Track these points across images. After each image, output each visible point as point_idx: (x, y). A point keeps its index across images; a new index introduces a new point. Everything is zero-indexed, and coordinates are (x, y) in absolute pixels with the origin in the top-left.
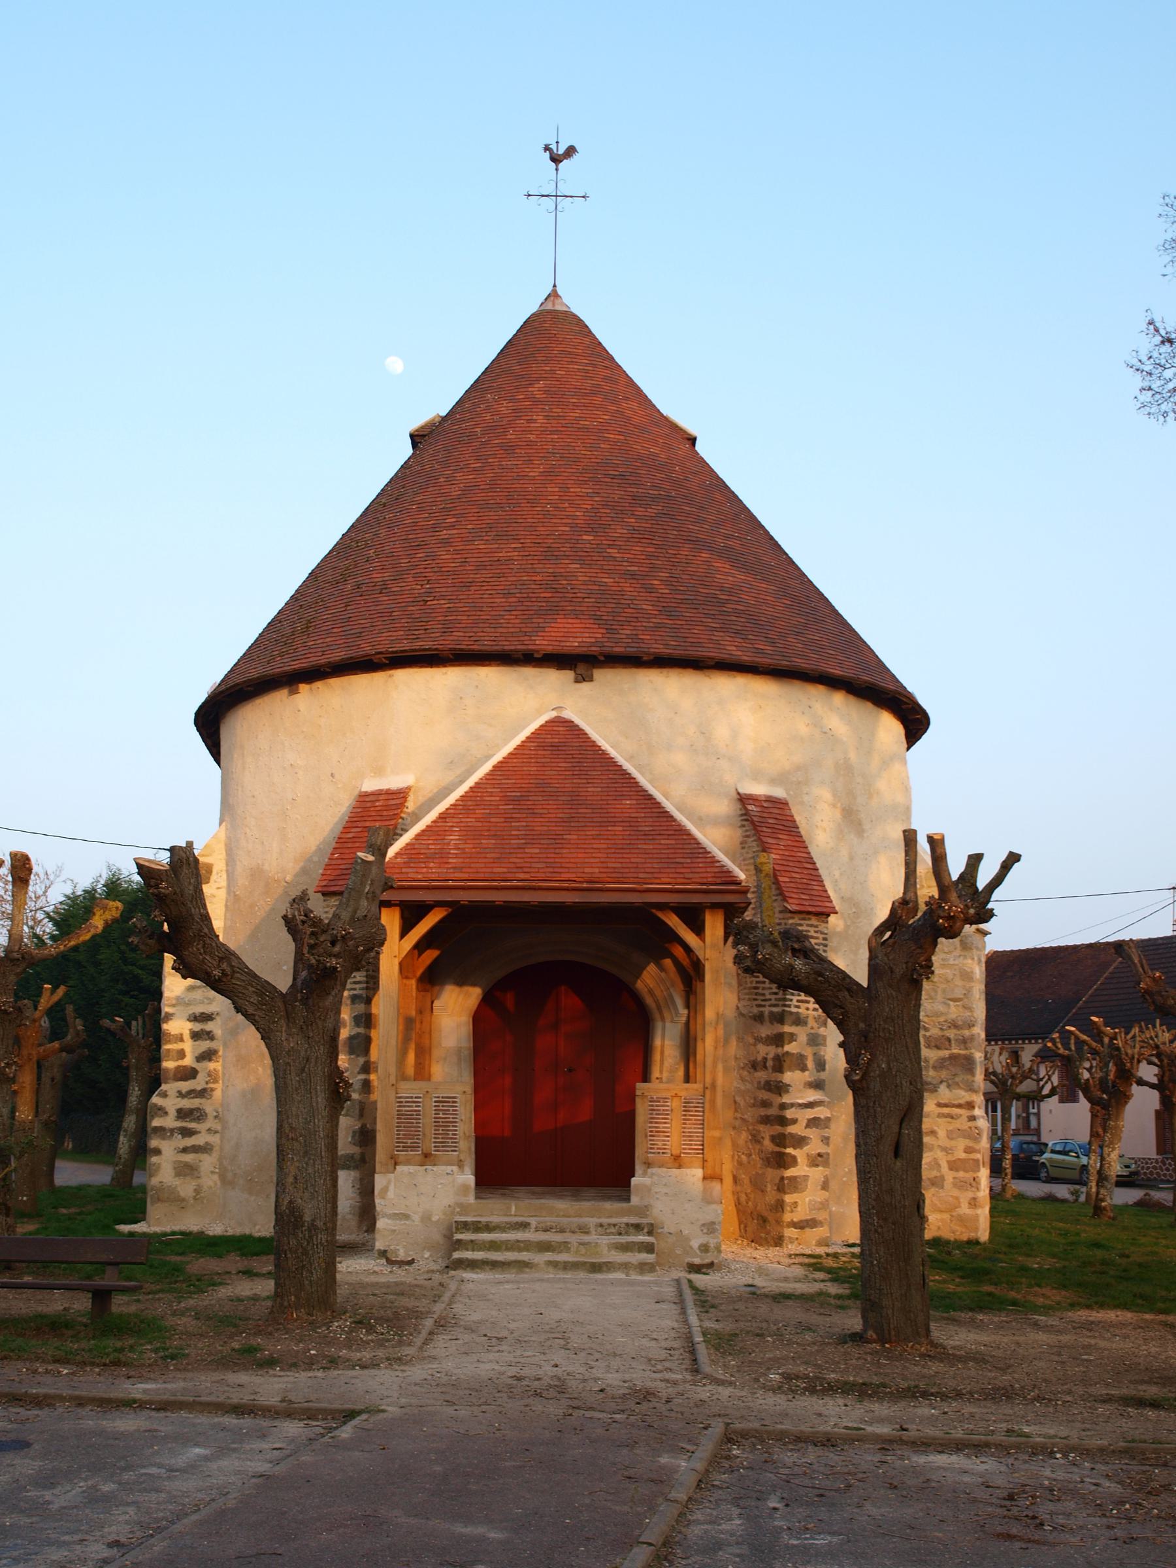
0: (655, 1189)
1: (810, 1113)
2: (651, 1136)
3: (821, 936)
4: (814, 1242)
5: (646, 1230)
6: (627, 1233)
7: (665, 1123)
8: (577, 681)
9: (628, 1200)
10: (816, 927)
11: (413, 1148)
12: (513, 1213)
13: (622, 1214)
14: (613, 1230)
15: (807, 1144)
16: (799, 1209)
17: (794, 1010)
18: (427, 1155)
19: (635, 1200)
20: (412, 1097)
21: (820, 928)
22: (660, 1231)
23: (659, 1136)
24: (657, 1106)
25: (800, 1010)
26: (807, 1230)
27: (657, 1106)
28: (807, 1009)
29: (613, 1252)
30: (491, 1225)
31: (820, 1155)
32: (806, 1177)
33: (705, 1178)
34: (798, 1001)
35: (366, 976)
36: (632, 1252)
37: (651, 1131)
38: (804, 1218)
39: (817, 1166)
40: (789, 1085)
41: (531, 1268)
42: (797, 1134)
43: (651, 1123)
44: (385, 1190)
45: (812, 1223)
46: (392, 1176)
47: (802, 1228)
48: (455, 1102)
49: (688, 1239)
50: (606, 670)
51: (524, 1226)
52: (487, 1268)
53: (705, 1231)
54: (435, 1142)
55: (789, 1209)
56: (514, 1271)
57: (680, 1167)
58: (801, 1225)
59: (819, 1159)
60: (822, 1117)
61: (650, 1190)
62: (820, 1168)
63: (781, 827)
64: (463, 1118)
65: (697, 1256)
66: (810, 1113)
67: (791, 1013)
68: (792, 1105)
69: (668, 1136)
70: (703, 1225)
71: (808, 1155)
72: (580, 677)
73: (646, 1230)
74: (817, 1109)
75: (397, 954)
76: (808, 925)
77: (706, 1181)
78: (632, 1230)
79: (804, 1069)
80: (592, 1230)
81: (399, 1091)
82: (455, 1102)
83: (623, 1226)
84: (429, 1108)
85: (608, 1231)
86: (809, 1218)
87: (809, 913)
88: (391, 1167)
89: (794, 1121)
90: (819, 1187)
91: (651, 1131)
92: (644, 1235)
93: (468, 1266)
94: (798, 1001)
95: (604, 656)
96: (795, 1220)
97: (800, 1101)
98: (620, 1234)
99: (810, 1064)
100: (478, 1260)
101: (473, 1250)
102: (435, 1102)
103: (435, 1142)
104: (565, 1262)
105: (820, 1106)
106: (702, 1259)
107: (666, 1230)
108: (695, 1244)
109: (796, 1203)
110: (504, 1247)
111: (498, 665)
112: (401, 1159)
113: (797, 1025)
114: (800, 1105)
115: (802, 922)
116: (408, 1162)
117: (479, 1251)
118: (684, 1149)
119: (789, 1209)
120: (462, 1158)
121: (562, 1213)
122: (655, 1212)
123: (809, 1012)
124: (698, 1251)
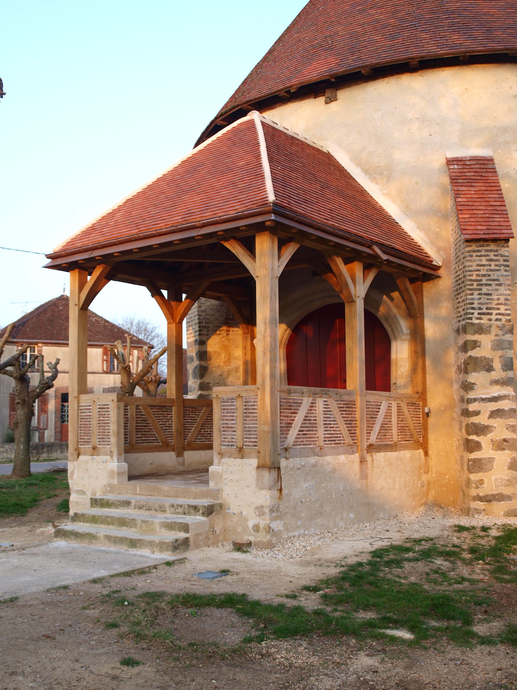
0: (224, 477)
1: (493, 406)
2: (224, 431)
3: (501, 259)
4: (502, 513)
5: (201, 512)
6: (189, 514)
7: (232, 420)
8: (327, 103)
9: (207, 482)
10: (497, 251)
11: (88, 442)
12: (138, 492)
13: (203, 495)
14: (180, 510)
15: (492, 431)
16: (485, 485)
17: (475, 321)
18: (94, 448)
19: (212, 484)
20: (86, 406)
21: (500, 252)
22: (227, 511)
23: (228, 431)
24: (227, 406)
25: (482, 321)
26: (495, 503)
27: (227, 406)
28: (490, 320)
29: (163, 530)
30: (110, 502)
31: (505, 440)
32: (491, 460)
33: (258, 467)
34: (479, 314)
35: (199, 327)
36: (174, 530)
37: (223, 427)
38: (491, 493)
39: (504, 449)
40: (474, 384)
41: (96, 540)
42: (480, 424)
43: (223, 420)
44: (73, 473)
45: (500, 498)
46: (76, 463)
47: (489, 501)
48: (108, 408)
49: (246, 520)
50: (346, 89)
51: (127, 503)
52: (73, 537)
53: (257, 513)
54: (99, 438)
55: (473, 485)
56: (87, 541)
57: (242, 457)
58: (487, 499)
59: (505, 443)
60: (506, 409)
61: (221, 477)
62: (507, 451)
63: (479, 178)
64: (112, 420)
65: (251, 535)
66: (493, 406)
67: (473, 324)
68: (475, 400)
69: (235, 431)
70: (256, 508)
71: (492, 441)
72: (328, 99)
73: (201, 512)
74: (500, 403)
75: (77, 303)
76: (487, 251)
77: (260, 470)
78: (192, 511)
79: (489, 369)
80: (167, 509)
81: (81, 401)
82: (108, 408)
83: (186, 507)
84: (95, 413)
85: (177, 511)
86: (495, 493)
87: (485, 240)
88: (76, 457)
89: (477, 413)
90: (506, 467)
91: (223, 427)
92: (200, 516)
93: (63, 535)
94: (479, 314)
95: (335, 78)
96: (481, 494)
97: (484, 396)
98: (185, 514)
99: (497, 365)
100: (68, 531)
101: (83, 522)
102: (99, 408)
103: (99, 438)
104: (115, 537)
105: (505, 399)
106: (256, 538)
107: (231, 511)
108: (251, 524)
109: (482, 480)
110: (100, 521)
111: (280, 106)
112: (82, 451)
113: (480, 334)
114: (483, 400)
115: (480, 249)
116: (85, 454)
117: (86, 523)
118: (246, 442)
119: (473, 485)
120: (112, 450)
121: (166, 494)
122: (224, 495)
123: (492, 322)
124: (252, 530)
